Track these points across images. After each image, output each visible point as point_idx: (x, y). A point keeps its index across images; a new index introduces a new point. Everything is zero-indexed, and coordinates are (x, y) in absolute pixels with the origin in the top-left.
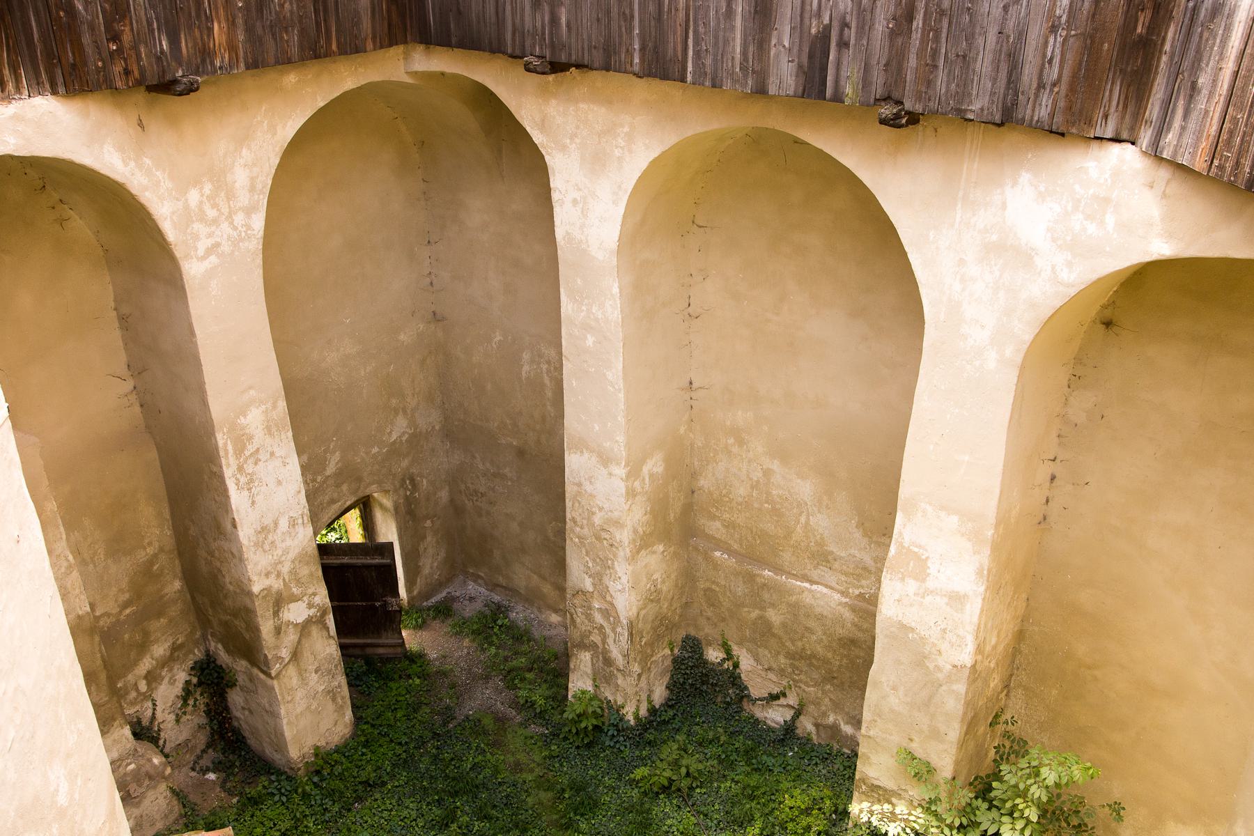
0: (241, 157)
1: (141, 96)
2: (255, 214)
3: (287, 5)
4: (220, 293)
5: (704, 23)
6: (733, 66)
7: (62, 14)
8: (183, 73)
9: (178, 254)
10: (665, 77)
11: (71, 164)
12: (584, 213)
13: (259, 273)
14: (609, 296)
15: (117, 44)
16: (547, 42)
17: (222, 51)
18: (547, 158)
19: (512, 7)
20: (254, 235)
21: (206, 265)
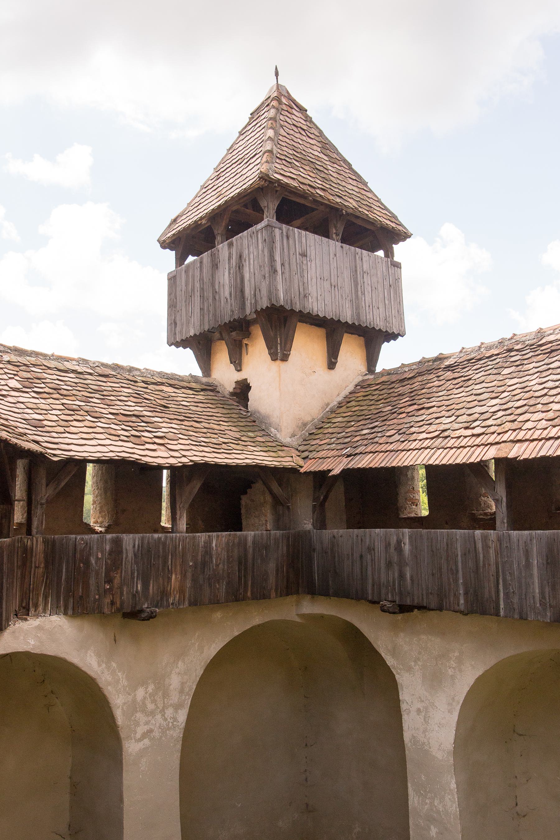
0: (177, 667)
1: (118, 620)
2: (181, 710)
3: (221, 566)
4: (147, 769)
5: (510, 573)
6: (534, 603)
7: (82, 565)
8: (148, 606)
9: (123, 735)
10: (483, 612)
11: (63, 661)
12: (426, 720)
13: (177, 756)
14: (448, 791)
15: (110, 585)
16: (397, 591)
17: (175, 592)
18: (397, 677)
19: (372, 569)
20: (178, 725)
21: (141, 745)
